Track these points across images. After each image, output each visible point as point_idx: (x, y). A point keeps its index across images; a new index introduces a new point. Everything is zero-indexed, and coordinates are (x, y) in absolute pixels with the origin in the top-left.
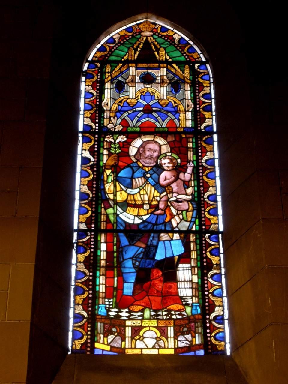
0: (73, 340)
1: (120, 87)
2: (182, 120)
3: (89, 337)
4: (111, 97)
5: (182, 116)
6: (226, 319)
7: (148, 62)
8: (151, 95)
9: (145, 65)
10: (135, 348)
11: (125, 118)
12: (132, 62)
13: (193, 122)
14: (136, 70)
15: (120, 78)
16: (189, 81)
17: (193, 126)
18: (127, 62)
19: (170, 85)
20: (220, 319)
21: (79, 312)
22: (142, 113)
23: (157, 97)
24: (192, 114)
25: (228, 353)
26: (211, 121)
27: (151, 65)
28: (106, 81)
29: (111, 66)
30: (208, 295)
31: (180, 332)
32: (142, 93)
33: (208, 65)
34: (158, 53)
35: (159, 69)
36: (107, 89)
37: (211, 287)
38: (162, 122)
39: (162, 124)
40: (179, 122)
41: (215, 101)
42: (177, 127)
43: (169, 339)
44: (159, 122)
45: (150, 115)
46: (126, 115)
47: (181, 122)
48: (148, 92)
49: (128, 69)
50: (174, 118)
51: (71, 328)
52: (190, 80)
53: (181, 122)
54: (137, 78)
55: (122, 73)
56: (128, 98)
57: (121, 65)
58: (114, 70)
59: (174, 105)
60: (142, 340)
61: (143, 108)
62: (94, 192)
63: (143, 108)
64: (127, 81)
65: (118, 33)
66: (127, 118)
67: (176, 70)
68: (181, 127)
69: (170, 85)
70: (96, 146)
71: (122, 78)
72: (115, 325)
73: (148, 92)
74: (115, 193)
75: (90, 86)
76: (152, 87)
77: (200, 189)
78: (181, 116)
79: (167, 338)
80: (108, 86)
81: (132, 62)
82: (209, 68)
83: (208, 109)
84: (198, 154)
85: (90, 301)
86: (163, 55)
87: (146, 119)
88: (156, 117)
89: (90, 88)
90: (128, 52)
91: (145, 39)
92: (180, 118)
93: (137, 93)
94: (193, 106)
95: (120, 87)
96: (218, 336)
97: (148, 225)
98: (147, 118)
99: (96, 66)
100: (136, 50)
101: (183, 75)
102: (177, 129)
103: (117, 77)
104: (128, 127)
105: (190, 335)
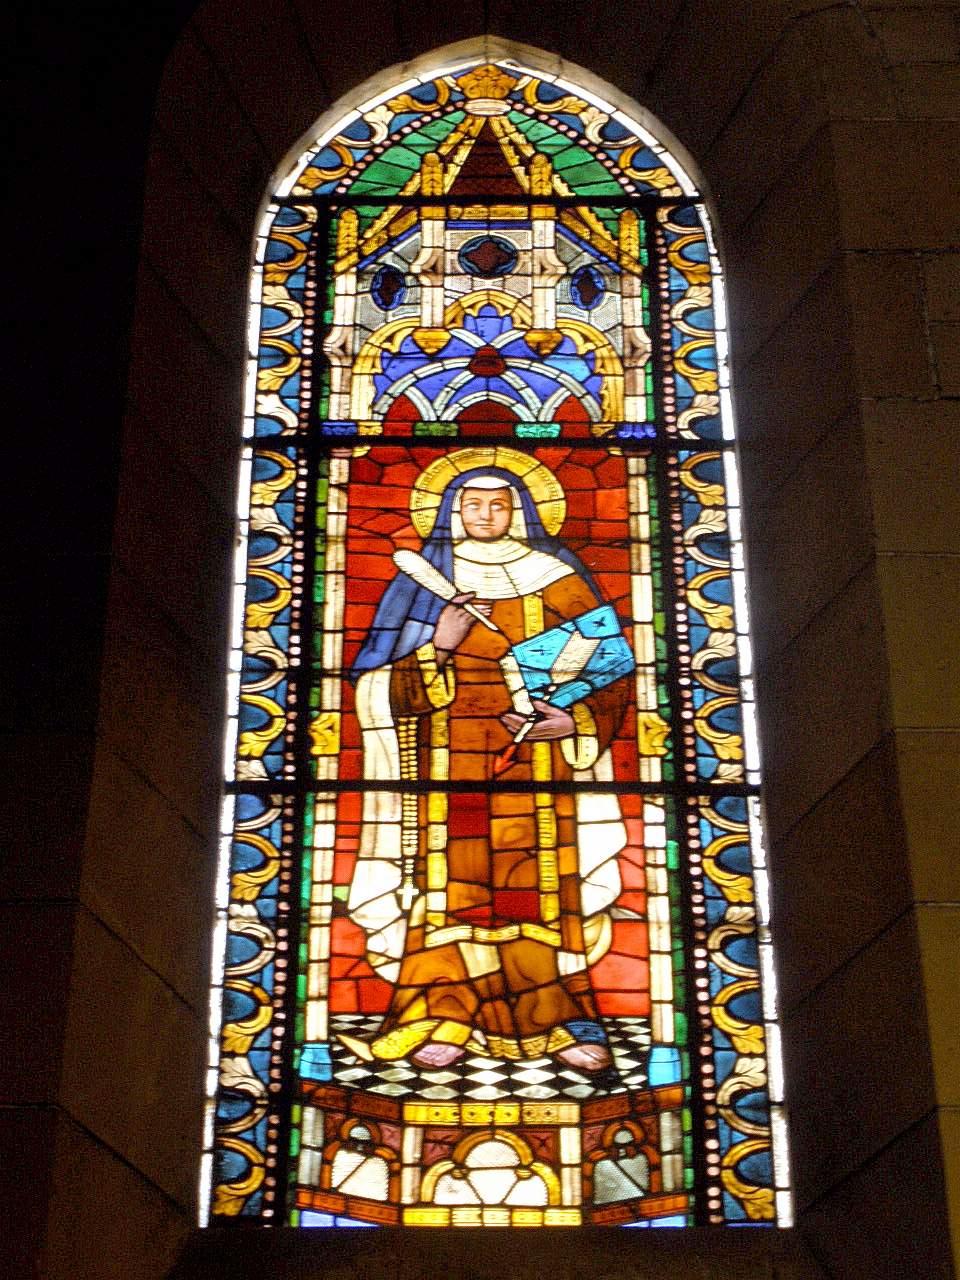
0: (218, 1178)
1: (388, 288)
2: (613, 398)
3: (307, 363)
4: (358, 322)
5: (611, 387)
6: (747, 677)
7: (489, 201)
8: (498, 317)
9: (477, 211)
10: (431, 1204)
11: (407, 393)
12: (433, 201)
13: (670, 816)
14: (446, 228)
15: (388, 259)
16: (638, 270)
17: (652, 417)
18: (419, 201)
19: (566, 282)
20: (718, 544)
21: (238, 1080)
22: (467, 376)
23: (523, 322)
24: (672, 905)
25: (785, 1221)
26: (717, 399)
27: (501, 211)
28: (340, 267)
29: (360, 217)
30: (690, 722)
31: (600, 1146)
32: (469, 311)
33: (701, 208)
34: (528, 173)
35: (527, 224)
36: (331, 572)
37: (702, 702)
38: (539, 405)
39: (539, 411)
40: (600, 405)
41: (775, 952)
42: (591, 423)
43: (566, 1172)
44: (527, 406)
45: (493, 382)
46: (410, 382)
47: (609, 406)
48: (489, 305)
49: (417, 227)
50: (584, 392)
51: (217, 974)
52: (638, 262)
53: (609, 406)
54: (451, 256)
55: (391, 242)
56: (418, 324)
57: (394, 209)
58: (370, 226)
59: (582, 350)
60: (464, 1177)
61: (468, 360)
62: (310, 303)
63: (468, 360)
64: (416, 269)
65: (384, 104)
66: (415, 395)
67: (592, 232)
68: (609, 422)
69: (566, 282)
70: (302, 485)
71: (397, 259)
72: (364, 1113)
73: (489, 305)
74: (373, 258)
75: (248, 902)
76: (503, 286)
77: (696, 999)
78: (606, 389)
79: (557, 1166)
80: (345, 283)
81: (433, 201)
82: (703, 215)
83: (748, 1009)
84: (707, 1205)
85: (268, 1213)
86: (539, 180)
87: (479, 396)
88: (517, 387)
89: (281, 292)
90: (419, 170)
91: (480, 122)
92: (603, 392)
93: (448, 310)
94: (649, 348)
95: (388, 288)
96: (687, 249)
97: (483, 1015)
98: (485, 393)
99: (304, 216)
100: (446, 161)
101: (615, 243)
102: (590, 427)
103: (377, 254)
104: (415, 422)
105: (641, 1159)
